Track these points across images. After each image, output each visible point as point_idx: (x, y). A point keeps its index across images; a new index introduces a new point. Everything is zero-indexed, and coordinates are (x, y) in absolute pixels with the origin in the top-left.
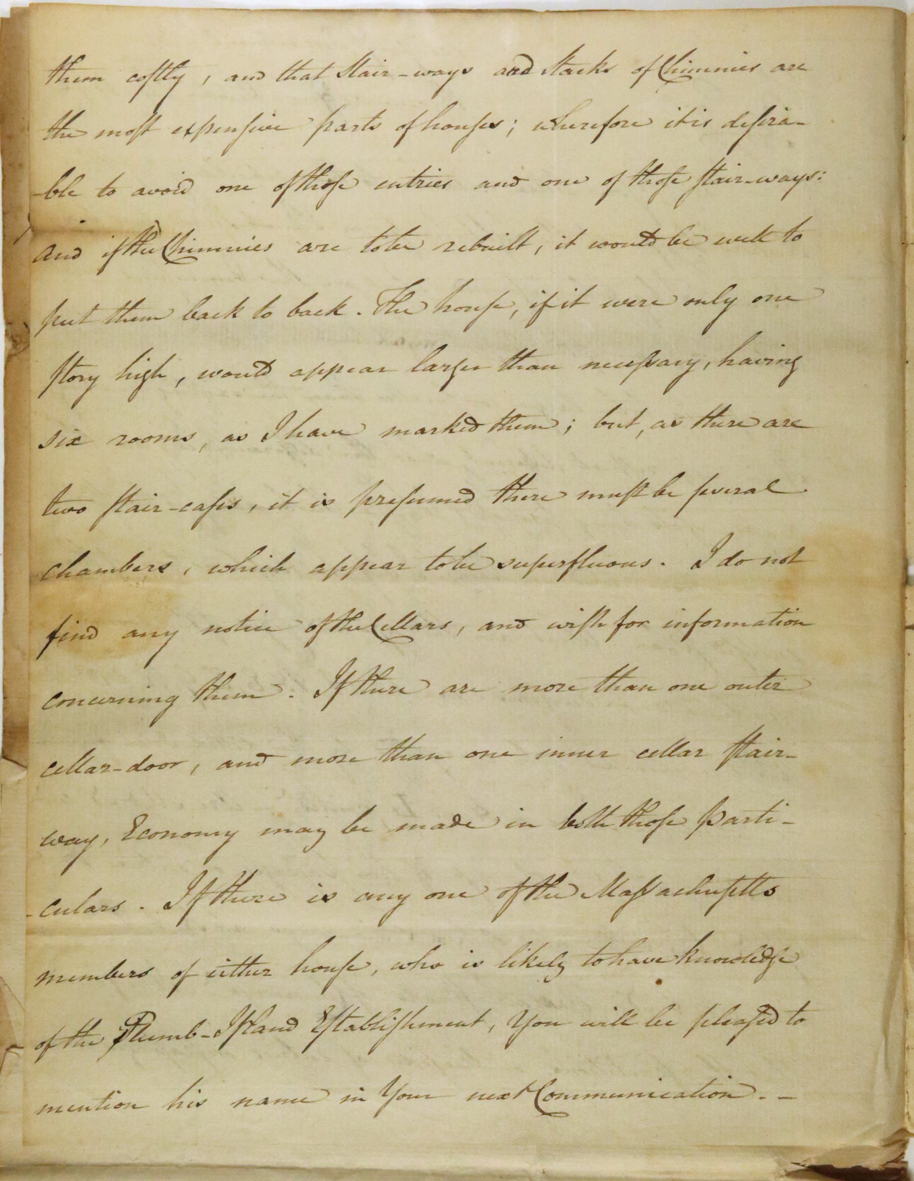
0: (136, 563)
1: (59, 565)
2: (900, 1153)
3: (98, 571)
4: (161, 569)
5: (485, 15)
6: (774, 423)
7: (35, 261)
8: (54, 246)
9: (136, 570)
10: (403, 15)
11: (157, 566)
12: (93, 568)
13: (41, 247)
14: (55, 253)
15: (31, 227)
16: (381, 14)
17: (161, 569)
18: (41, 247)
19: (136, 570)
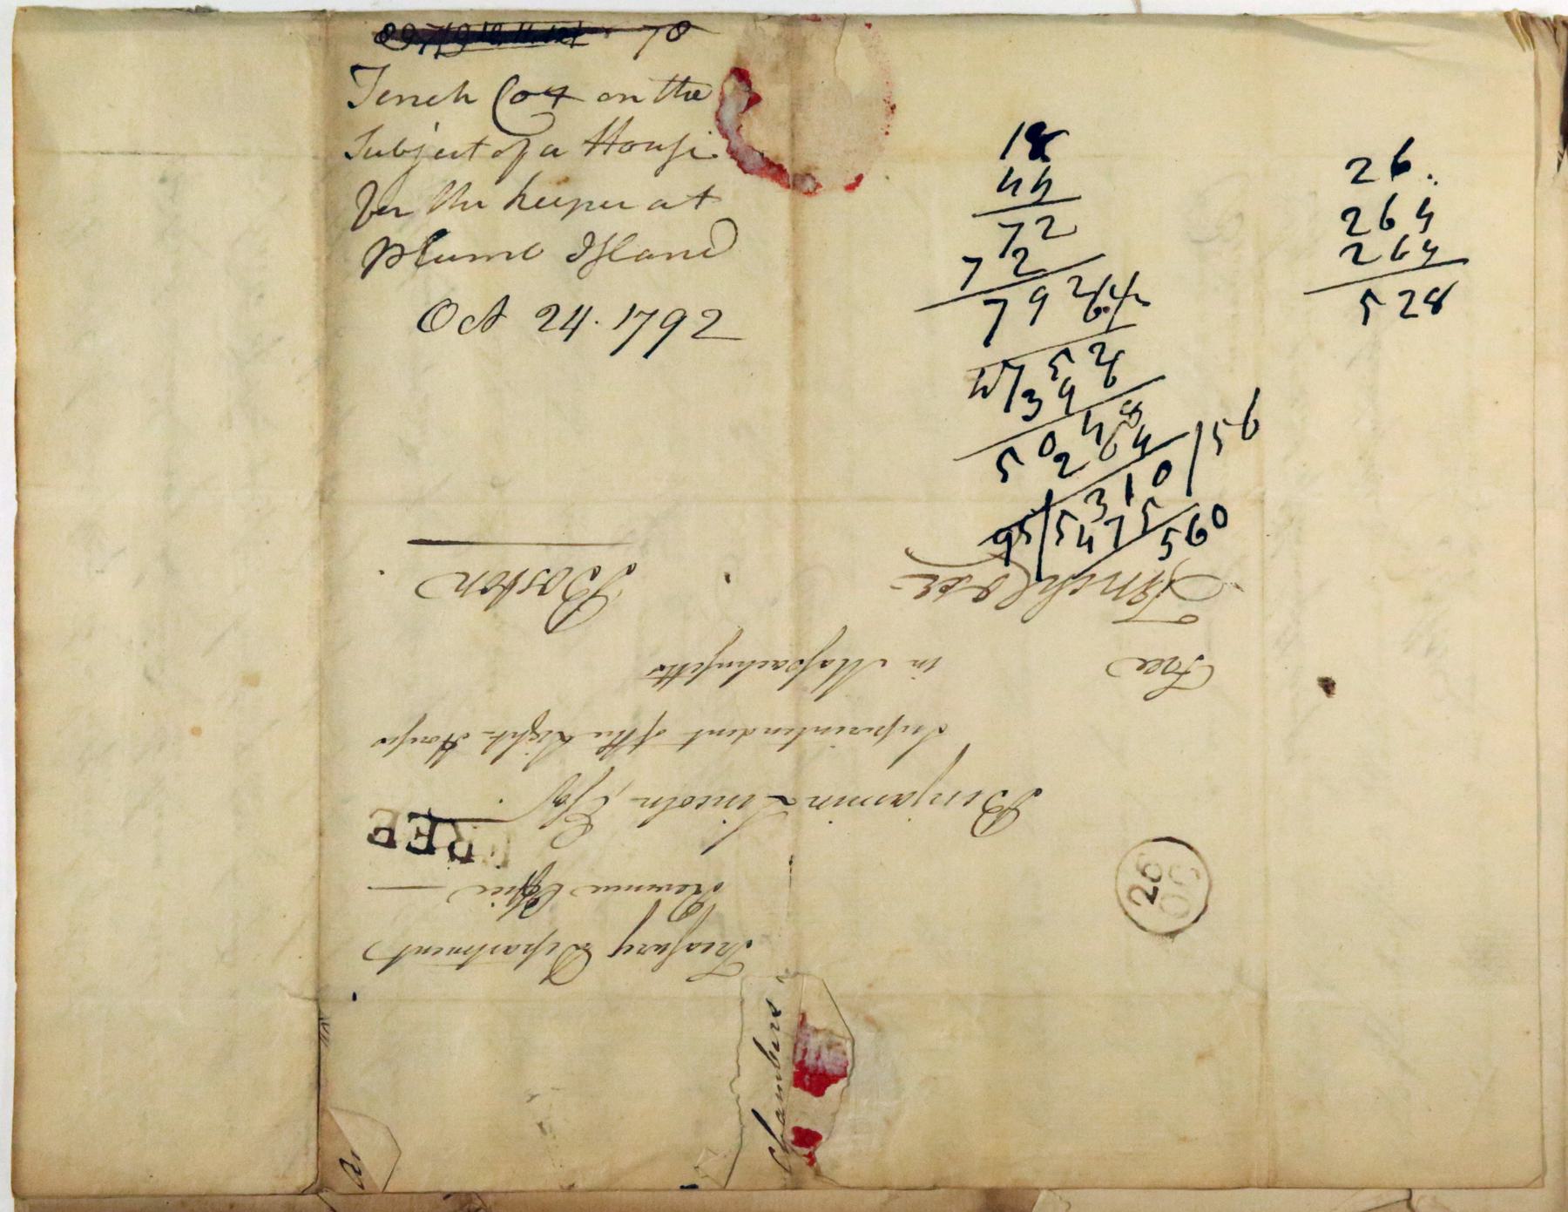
0: (768, 1047)
1: (771, 1150)
2: (1543, 27)
3: (779, 1097)
4: (776, 1014)
5: (24, 556)
6: (509, 257)
7: (362, 1187)
8: (342, 1162)
9: (777, 1047)
10: (1219, 1185)
11: (772, 1019)
12: (776, 1104)
13: (345, 1181)
14: (350, 1160)
15: (317, 1193)
16: (30, 676)
17: (776, 1014)
18: (345, 1181)
19: (777, 1047)
